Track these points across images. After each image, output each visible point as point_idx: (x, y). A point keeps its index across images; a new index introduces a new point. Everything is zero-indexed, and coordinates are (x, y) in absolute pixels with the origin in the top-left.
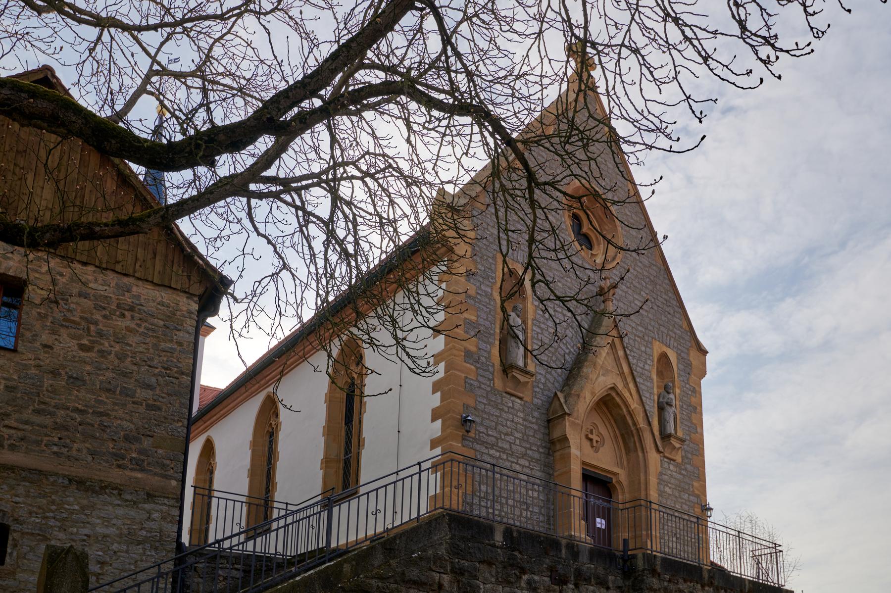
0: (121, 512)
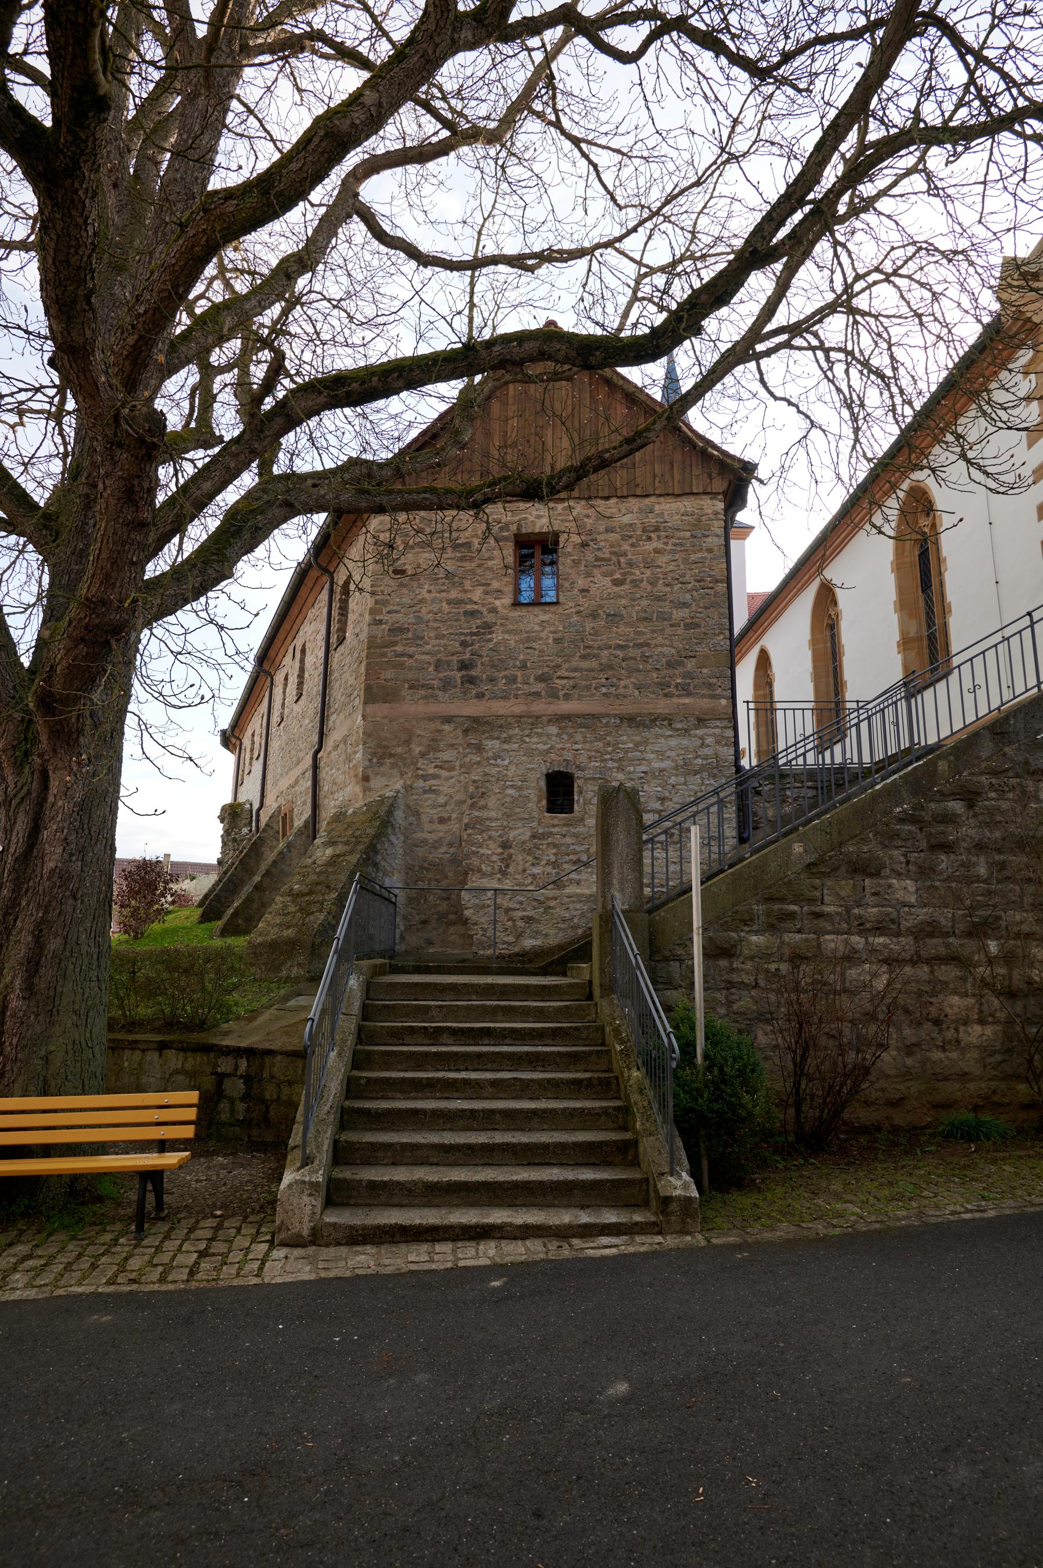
0: (673, 742)
